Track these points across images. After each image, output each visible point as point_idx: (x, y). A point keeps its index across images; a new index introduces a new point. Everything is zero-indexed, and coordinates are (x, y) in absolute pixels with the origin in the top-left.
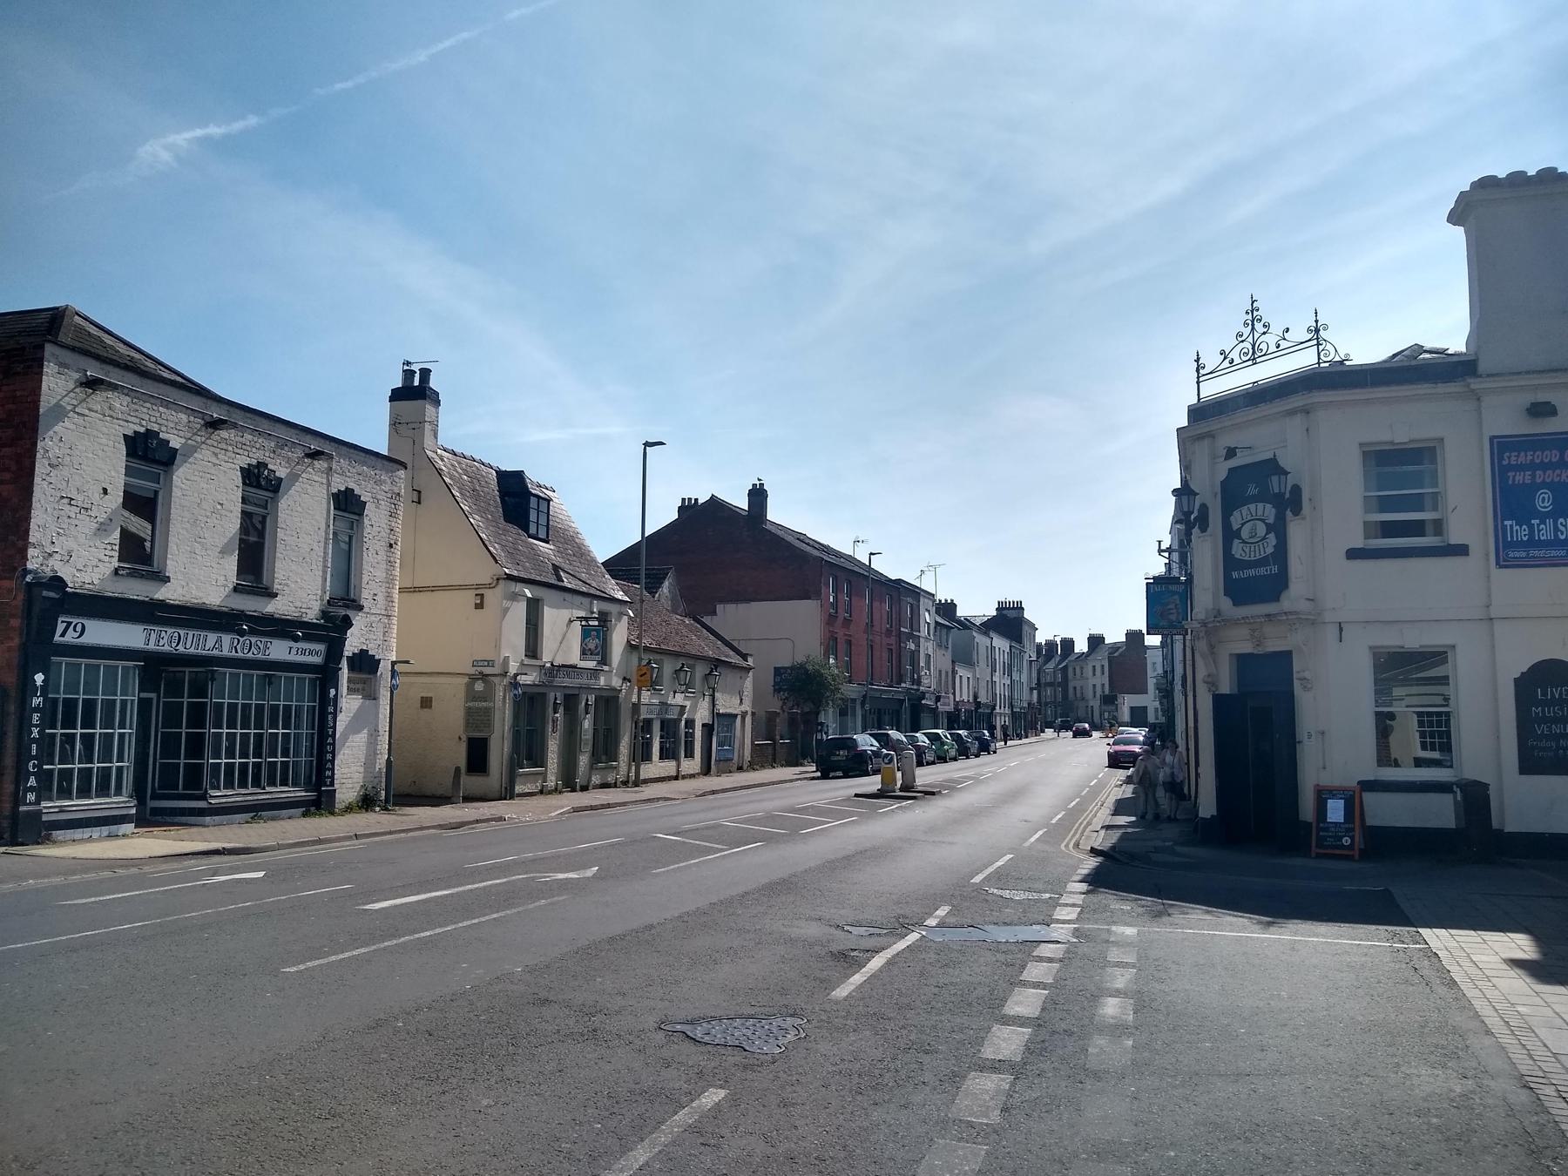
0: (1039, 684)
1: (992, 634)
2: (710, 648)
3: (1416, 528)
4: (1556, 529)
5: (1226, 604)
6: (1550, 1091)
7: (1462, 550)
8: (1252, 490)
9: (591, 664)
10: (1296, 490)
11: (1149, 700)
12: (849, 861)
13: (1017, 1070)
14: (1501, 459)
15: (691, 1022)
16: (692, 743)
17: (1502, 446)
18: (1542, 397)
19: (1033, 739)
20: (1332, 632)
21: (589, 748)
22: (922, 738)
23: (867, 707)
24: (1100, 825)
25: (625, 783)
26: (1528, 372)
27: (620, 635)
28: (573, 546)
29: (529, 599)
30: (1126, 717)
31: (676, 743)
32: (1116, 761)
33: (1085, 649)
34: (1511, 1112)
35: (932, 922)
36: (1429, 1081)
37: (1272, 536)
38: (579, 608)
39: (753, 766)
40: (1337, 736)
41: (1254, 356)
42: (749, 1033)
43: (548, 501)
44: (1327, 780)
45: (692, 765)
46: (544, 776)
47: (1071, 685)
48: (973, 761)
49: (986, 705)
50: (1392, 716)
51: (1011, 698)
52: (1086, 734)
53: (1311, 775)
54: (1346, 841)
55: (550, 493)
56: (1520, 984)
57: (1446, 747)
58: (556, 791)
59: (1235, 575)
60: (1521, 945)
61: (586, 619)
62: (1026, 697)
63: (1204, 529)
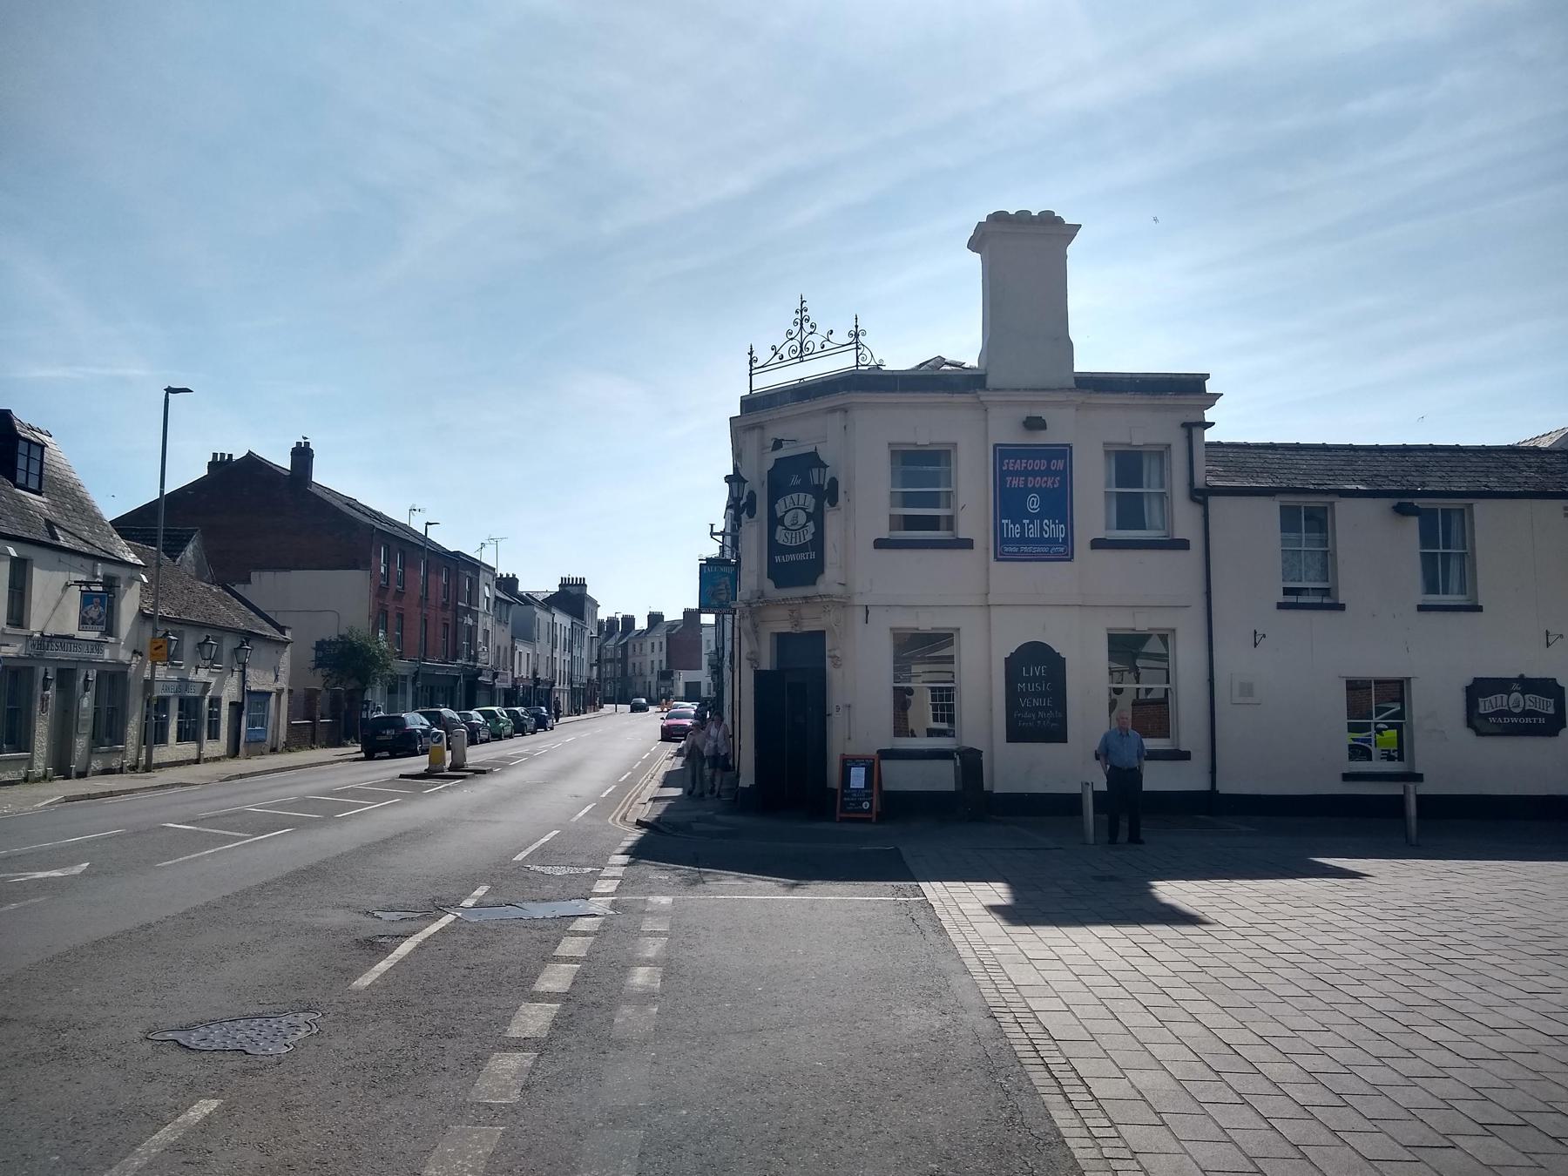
0: (599, 660)
1: (554, 610)
2: (238, 618)
3: (932, 523)
4: (1042, 529)
5: (769, 585)
6: (1009, 1018)
7: (967, 544)
8: (795, 481)
9: (93, 635)
10: (834, 483)
11: (703, 676)
12: (385, 844)
13: (540, 1046)
14: (1002, 464)
15: (187, 1028)
16: (217, 723)
17: (1003, 453)
18: (1036, 413)
19: (592, 715)
20: (861, 613)
21: (88, 729)
22: (476, 716)
23: (419, 684)
24: (648, 797)
25: (134, 768)
26: (1061, 389)
27: (130, 604)
28: (74, 501)
29: (13, 558)
30: (681, 693)
31: (198, 723)
32: (668, 735)
33: (645, 627)
34: (978, 1040)
35: (469, 903)
36: (915, 1020)
37: (811, 524)
38: (80, 570)
39: (288, 748)
40: (861, 706)
41: (802, 354)
42: (254, 1034)
43: (42, 446)
44: (853, 749)
45: (219, 747)
46: (30, 762)
47: (630, 661)
48: (529, 738)
49: (545, 682)
50: (910, 691)
51: (571, 674)
52: (643, 709)
53: (838, 746)
54: (866, 805)
55: (46, 438)
56: (994, 927)
57: (951, 720)
58: (45, 778)
60: (999, 893)
61: (87, 584)
62: (585, 673)
63: (751, 516)
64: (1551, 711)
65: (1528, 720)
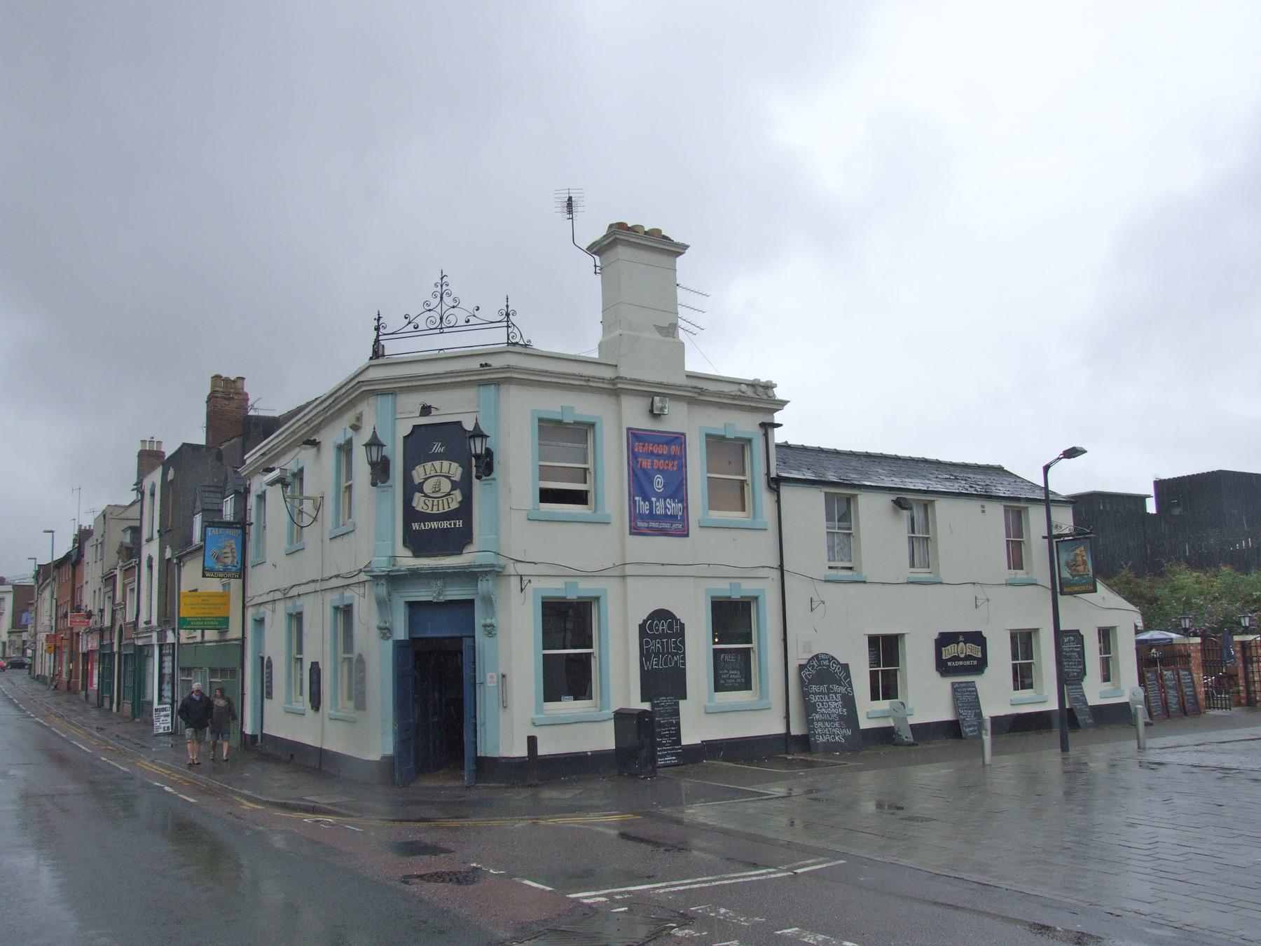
20: (515, 582)
59: (415, 526)
64: (980, 655)
65: (968, 663)
